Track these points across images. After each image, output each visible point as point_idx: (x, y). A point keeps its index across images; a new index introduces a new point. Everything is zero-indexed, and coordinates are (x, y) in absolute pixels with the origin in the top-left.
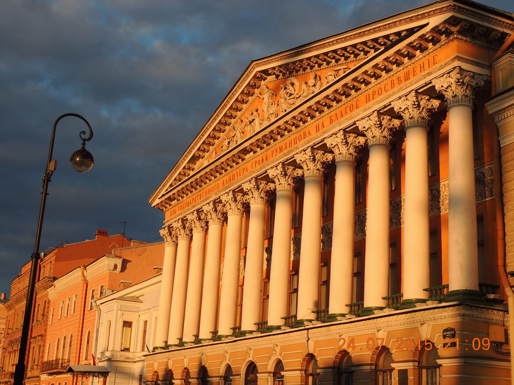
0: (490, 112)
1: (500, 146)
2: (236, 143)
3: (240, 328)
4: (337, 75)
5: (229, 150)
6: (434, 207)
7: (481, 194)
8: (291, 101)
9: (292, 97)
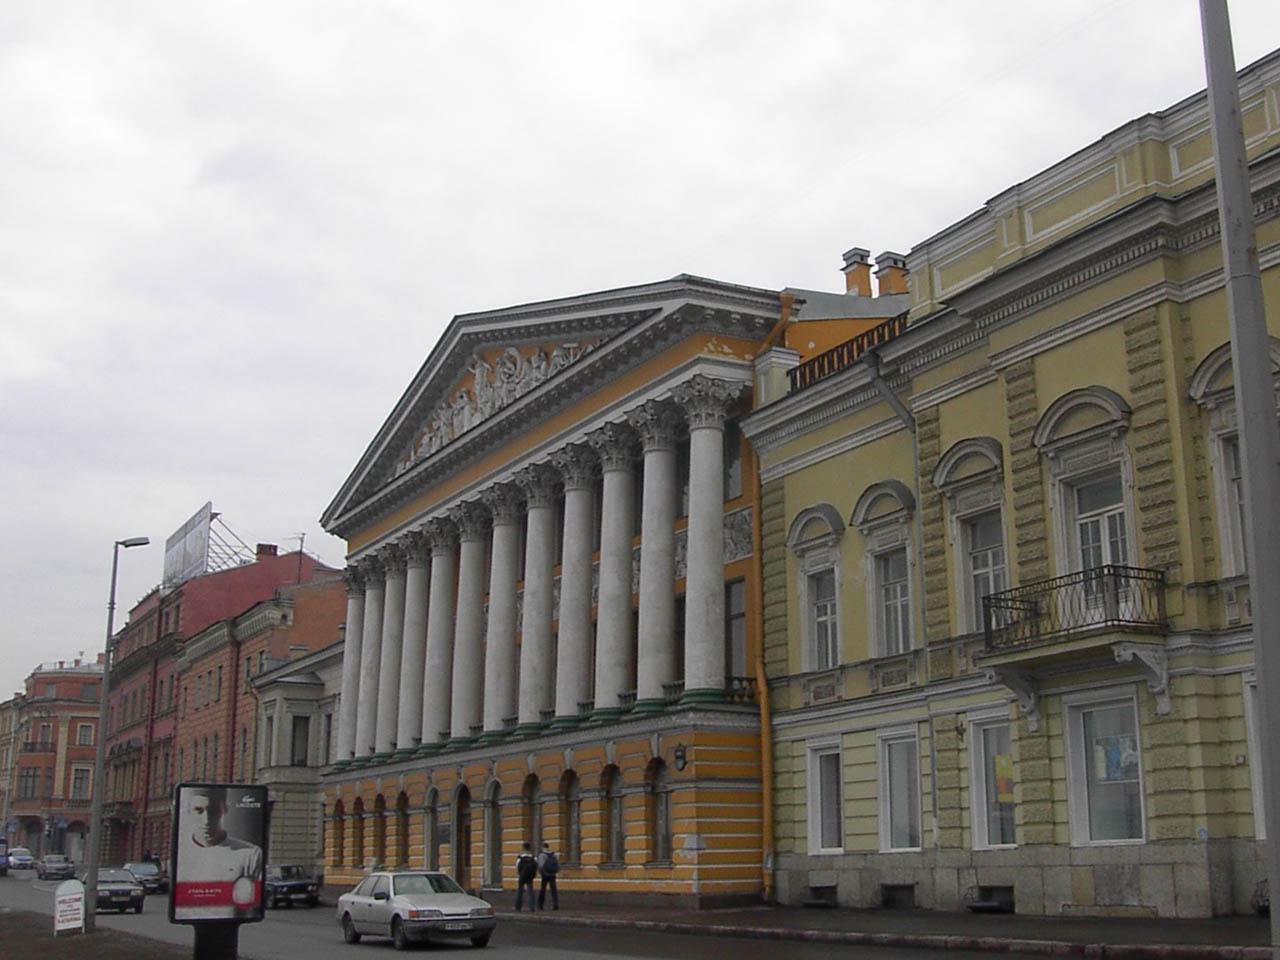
0: (747, 436)
3: (635, 696)
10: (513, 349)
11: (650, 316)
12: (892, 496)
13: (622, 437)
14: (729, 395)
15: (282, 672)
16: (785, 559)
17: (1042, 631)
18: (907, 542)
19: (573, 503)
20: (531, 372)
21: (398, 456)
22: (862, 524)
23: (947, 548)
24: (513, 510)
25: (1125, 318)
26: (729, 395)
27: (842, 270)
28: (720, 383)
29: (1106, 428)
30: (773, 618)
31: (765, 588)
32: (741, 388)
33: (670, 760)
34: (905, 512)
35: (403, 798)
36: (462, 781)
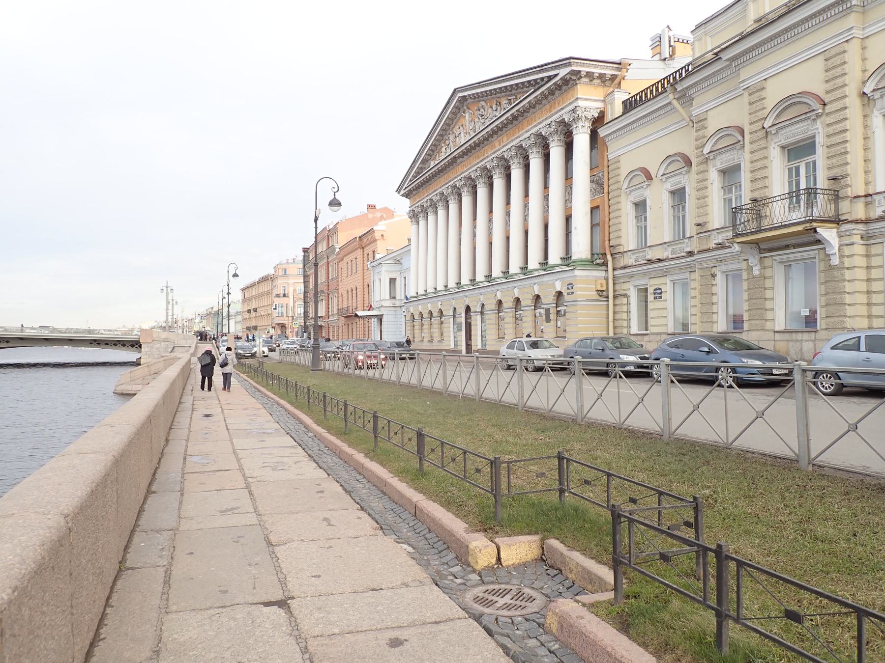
0: (601, 136)
9: (483, 117)
11: (553, 78)
12: (678, 161)
13: (538, 141)
15: (384, 259)
17: (762, 225)
18: (686, 184)
19: (482, 192)
20: (493, 113)
23: (709, 186)
24: (486, 180)
25: (825, 51)
29: (808, 115)
30: (614, 225)
33: (565, 291)
34: (686, 168)
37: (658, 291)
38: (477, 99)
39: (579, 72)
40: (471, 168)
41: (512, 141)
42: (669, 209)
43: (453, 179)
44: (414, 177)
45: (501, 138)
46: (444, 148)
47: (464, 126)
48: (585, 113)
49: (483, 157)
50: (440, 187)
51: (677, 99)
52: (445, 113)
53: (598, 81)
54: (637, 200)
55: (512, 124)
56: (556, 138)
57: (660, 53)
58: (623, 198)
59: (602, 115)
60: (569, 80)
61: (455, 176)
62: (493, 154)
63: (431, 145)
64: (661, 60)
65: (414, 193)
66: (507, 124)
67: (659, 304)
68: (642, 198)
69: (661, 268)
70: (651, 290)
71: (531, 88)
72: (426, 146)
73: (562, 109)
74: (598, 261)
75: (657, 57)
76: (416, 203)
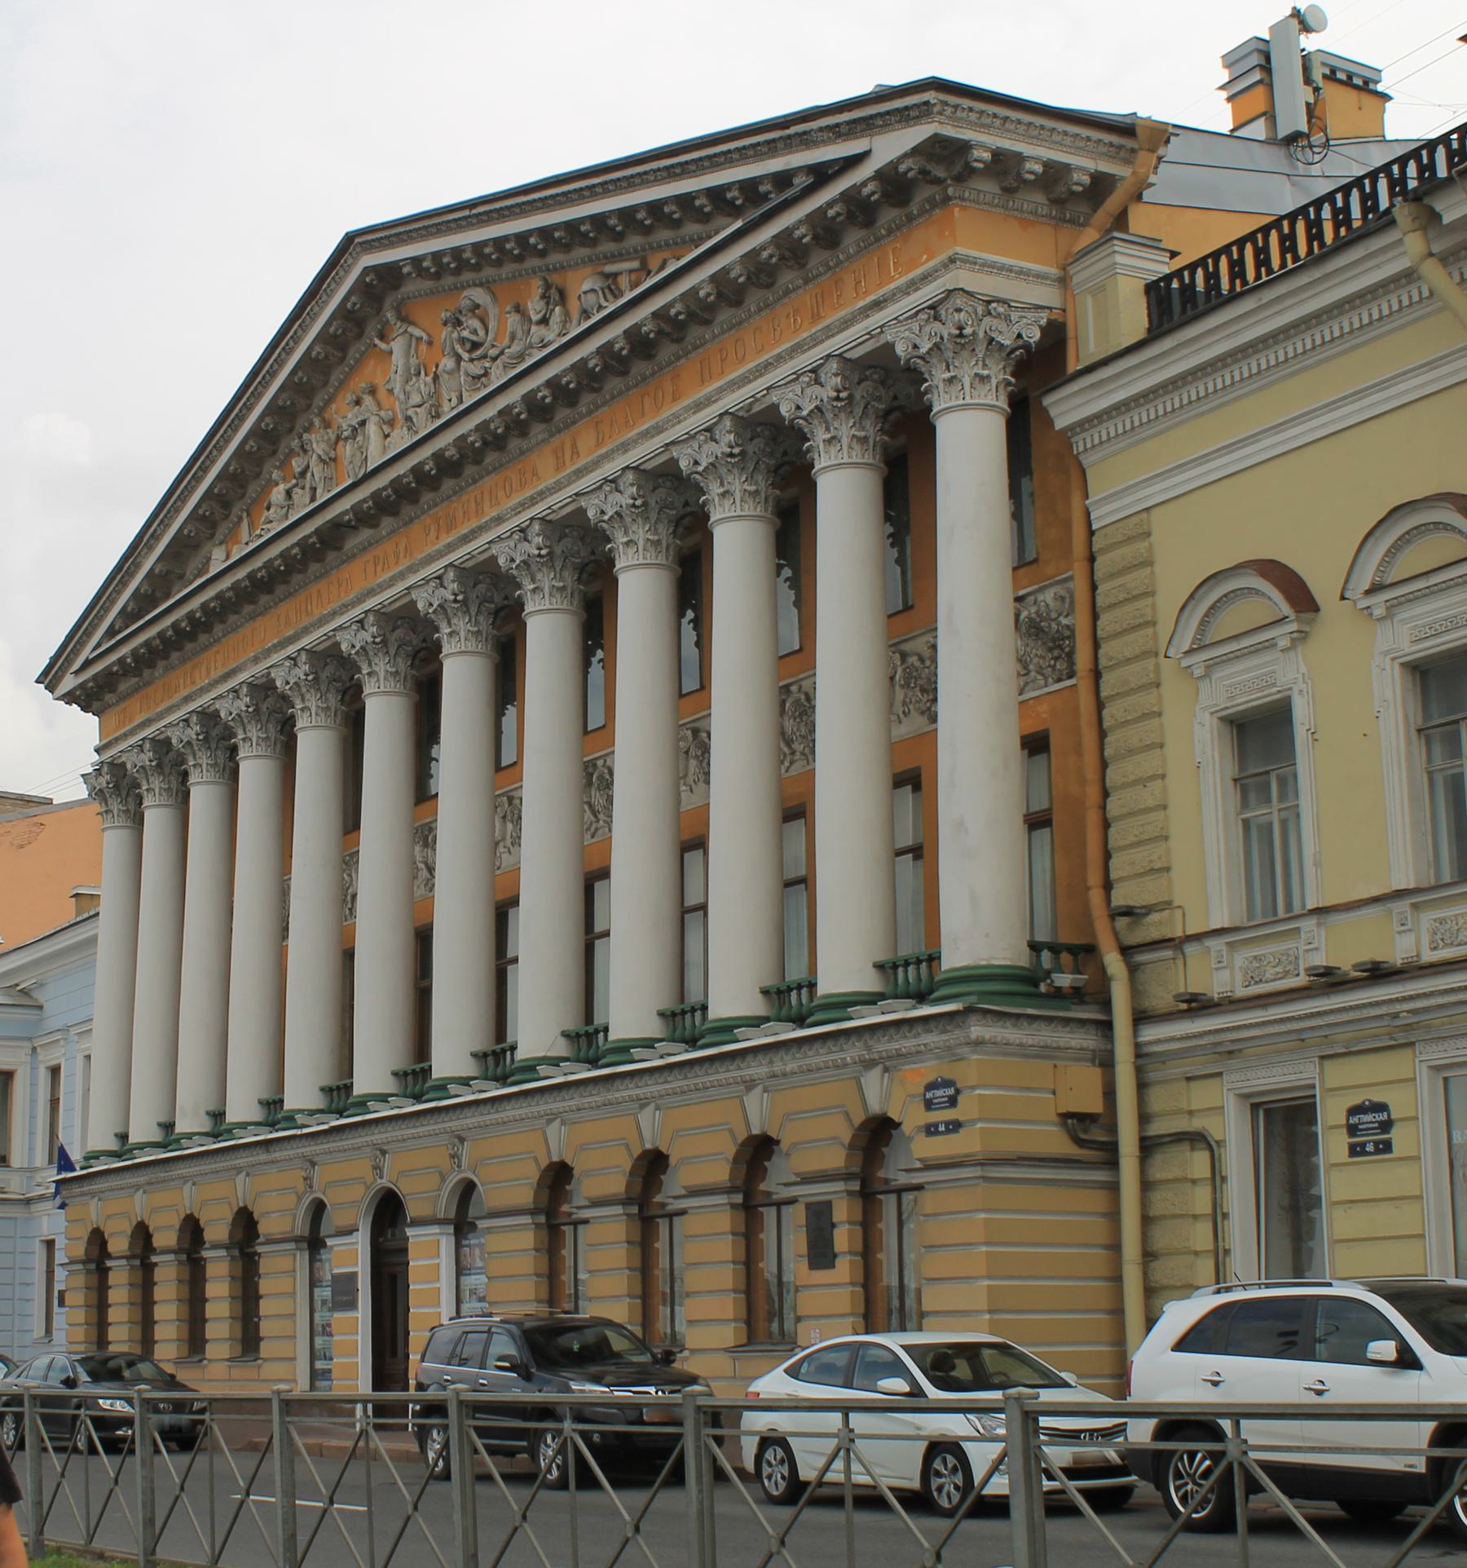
1: (1090, 525)
2: (313, 499)
3: (349, 1088)
4: (610, 289)
5: (462, 407)
6: (911, 707)
7: (1041, 668)
8: (476, 369)
10: (479, 290)
12: (1257, 592)
13: (751, 448)
14: (1019, 336)
16: (1158, 685)
21: (212, 536)
22: (1368, 592)
26: (1019, 336)
27: (1222, 88)
28: (1001, 310)
31: (1108, 752)
32: (1043, 322)
35: (246, 1223)
36: (384, 1182)
37: (1368, 1118)
38: (448, 281)
39: (965, 147)
40: (412, 569)
41: (625, 447)
42: (1409, 742)
43: (322, 621)
44: (127, 616)
45: (566, 437)
46: (282, 487)
47: (382, 394)
48: (987, 320)
49: (474, 524)
50: (256, 660)
51: (1445, 259)
52: (297, 340)
53: (1037, 199)
54: (1245, 701)
55: (624, 373)
56: (546, 580)
57: (1270, 116)
58: (1172, 692)
59: (1056, 336)
60: (913, 181)
61: (335, 605)
62: (523, 506)
63: (219, 478)
64: (1272, 141)
65: (123, 687)
66: (289, 571)
67: (1372, 1177)
68: (1269, 696)
69: (1383, 1010)
70: (1331, 1114)
71: (720, 220)
72: (197, 479)
73: (878, 305)
74: (1064, 980)
75: (1258, 130)
76: (132, 732)
